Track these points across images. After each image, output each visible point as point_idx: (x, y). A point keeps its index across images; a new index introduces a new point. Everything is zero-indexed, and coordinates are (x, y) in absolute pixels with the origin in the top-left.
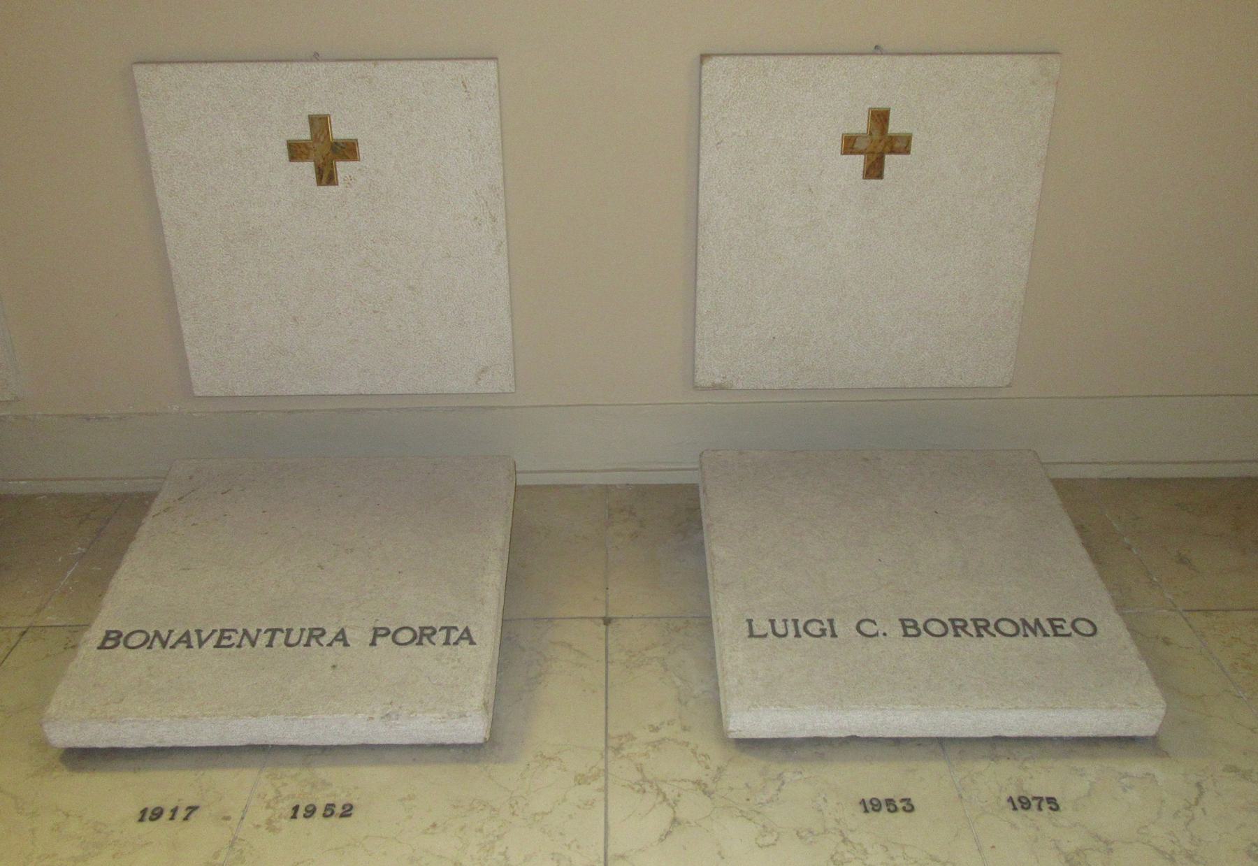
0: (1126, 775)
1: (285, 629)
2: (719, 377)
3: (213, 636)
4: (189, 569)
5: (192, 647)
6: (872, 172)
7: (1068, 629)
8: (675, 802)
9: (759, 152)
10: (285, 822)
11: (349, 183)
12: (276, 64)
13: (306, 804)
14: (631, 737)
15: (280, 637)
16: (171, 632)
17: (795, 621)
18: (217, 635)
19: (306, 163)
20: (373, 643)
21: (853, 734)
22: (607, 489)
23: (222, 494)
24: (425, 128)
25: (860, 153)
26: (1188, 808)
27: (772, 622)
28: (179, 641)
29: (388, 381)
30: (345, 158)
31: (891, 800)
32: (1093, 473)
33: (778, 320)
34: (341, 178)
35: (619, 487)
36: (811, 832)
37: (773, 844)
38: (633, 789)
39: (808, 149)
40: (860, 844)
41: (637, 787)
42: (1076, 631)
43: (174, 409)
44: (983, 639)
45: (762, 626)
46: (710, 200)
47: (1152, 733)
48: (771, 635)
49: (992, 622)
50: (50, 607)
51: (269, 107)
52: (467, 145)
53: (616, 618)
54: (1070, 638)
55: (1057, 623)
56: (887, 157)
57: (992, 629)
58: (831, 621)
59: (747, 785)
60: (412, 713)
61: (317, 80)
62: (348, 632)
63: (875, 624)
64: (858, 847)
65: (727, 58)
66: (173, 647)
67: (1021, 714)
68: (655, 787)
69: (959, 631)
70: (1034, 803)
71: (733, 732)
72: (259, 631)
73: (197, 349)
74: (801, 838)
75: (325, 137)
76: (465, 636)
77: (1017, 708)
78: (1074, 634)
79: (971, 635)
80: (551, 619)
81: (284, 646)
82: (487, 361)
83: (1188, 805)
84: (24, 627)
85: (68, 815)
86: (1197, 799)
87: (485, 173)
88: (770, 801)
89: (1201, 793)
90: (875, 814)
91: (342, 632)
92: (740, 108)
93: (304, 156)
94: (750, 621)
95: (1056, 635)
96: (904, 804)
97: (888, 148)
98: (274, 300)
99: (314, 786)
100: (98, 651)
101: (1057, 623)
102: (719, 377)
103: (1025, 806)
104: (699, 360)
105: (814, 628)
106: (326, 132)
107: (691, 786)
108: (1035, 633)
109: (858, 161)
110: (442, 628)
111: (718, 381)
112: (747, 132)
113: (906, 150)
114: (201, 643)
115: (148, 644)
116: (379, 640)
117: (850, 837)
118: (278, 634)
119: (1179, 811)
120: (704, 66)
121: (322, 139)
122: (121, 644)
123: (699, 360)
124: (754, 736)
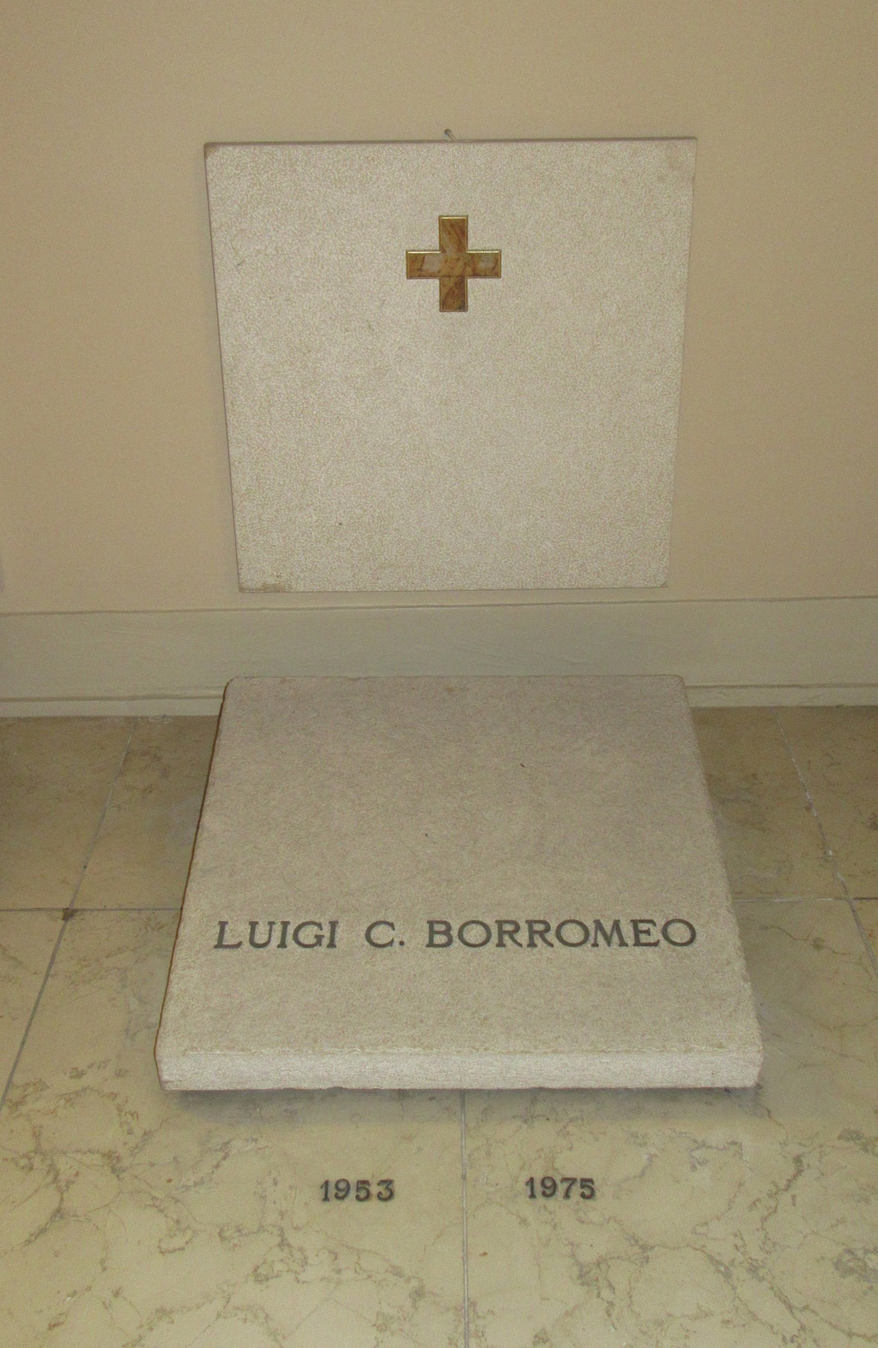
0: (703, 1145)
2: (272, 575)
6: (450, 301)
7: (656, 935)
8: (69, 1183)
9: (296, 277)
12: (446, 145)
14: (41, 1086)
17: (285, 924)
21: (336, 1084)
22: (133, 722)
25: (432, 276)
26: (771, 1196)
27: (253, 925)
31: (365, 1182)
32: (792, 699)
33: (344, 500)
35: (151, 721)
36: (239, 1231)
37: (182, 1249)
38: (17, 1164)
39: (361, 271)
40: (301, 1250)
41: (23, 1162)
42: (666, 937)
44: (535, 950)
45: (238, 931)
46: (236, 340)
47: (749, 1083)
48: (246, 945)
49: (554, 925)
53: (83, 910)
54: (657, 949)
55: (643, 927)
56: (471, 282)
57: (551, 936)
58: (334, 925)
59: (175, 1158)
63: (394, 929)
64: (297, 1255)
65: (238, 149)
67: (561, 1059)
68: (48, 1162)
69: (506, 938)
70: (562, 1188)
71: (172, 1082)
74: (222, 1238)
77: (555, 1052)
78: (664, 943)
79: (520, 945)
83: (774, 1190)
86: (789, 1181)
88: (200, 1183)
89: (799, 1172)
90: (338, 1202)
92: (264, 216)
94: (223, 924)
95: (638, 943)
96: (381, 1189)
97: (469, 270)
101: (643, 927)
102: (272, 575)
103: (548, 1192)
104: (242, 553)
105: (308, 935)
107: (96, 1159)
108: (608, 941)
109: (431, 288)
111: (271, 581)
112: (276, 249)
113: (495, 272)
117: (294, 1239)
119: (759, 1200)
120: (209, 159)
122: (456, 940)
123: (242, 553)
124: (201, 1087)
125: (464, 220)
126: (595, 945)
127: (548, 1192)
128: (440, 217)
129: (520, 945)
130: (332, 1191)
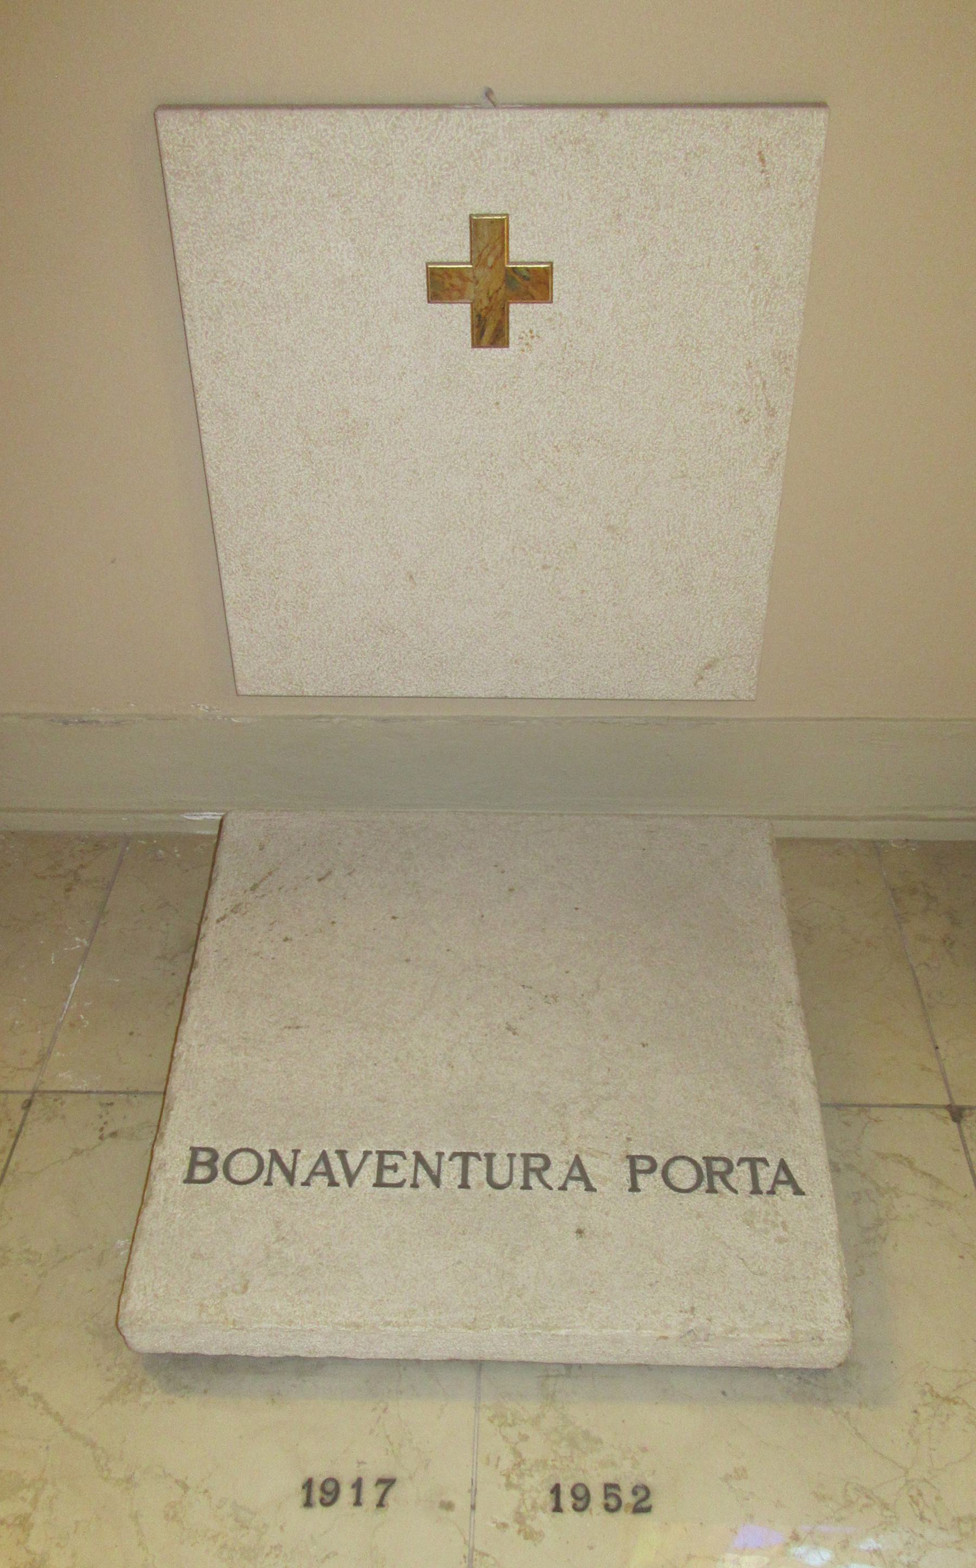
1: (481, 1153)
3: (367, 1162)
4: (298, 1027)
5: (337, 1185)
10: (544, 1520)
11: (527, 344)
12: (418, 113)
13: (571, 1483)
15: (477, 1169)
16: (296, 1152)
18: (373, 1159)
19: (455, 306)
20: (634, 1188)
23: (320, 880)
24: (675, 241)
28: (313, 1173)
29: (551, 677)
30: (527, 297)
34: (514, 334)
43: (201, 709)
50: (58, 1054)
51: (400, 198)
52: (746, 275)
60: (731, 1332)
61: (493, 146)
62: (586, 1161)
66: (306, 1184)
72: (440, 1155)
73: (246, 622)
75: (496, 258)
76: (783, 1177)
80: (864, 1107)
81: (487, 1187)
82: (719, 650)
84: (27, 1092)
85: (186, 1488)
87: (771, 329)
91: (578, 1161)
93: (455, 294)
98: (379, 544)
99: (572, 1442)
100: (186, 1186)
106: (499, 247)
110: (742, 1160)
114: (351, 1178)
115: (264, 1175)
116: (640, 1178)
118: (473, 1163)
121: (491, 261)
122: (221, 1175)
125: (502, 220)
126: (268, 1183)
127: (580, 1504)
128: (471, 216)
129: (551, 1188)
130: (317, 1494)
